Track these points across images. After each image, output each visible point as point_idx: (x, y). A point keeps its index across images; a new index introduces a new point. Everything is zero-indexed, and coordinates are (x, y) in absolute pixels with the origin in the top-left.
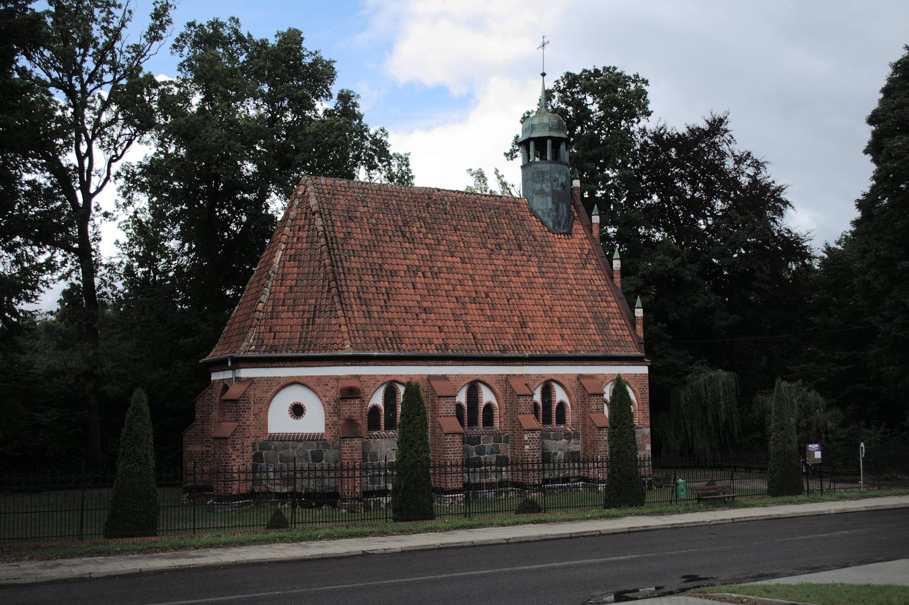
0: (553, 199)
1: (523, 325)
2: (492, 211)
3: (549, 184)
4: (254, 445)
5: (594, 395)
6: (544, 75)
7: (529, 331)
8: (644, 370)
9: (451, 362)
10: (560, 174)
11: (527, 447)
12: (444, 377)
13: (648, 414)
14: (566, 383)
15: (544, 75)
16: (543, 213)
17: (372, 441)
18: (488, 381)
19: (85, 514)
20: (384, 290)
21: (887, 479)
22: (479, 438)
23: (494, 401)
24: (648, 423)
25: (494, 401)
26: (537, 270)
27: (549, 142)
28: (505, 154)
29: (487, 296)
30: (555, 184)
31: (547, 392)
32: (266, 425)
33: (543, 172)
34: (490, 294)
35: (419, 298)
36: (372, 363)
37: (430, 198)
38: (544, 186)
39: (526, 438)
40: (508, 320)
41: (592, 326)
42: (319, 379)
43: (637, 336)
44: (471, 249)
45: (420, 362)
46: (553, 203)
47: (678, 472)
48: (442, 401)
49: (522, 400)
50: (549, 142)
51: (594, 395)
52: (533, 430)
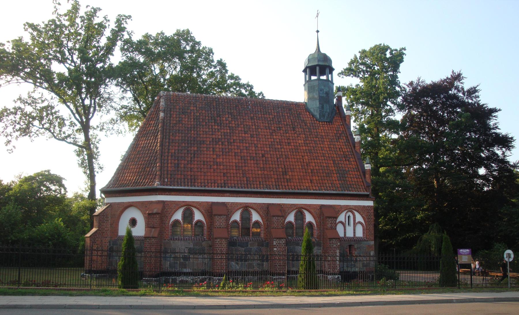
0: (319, 101)
1: (285, 173)
2: (280, 109)
3: (317, 93)
4: (110, 242)
5: (329, 217)
6: (318, 31)
7: (288, 177)
8: (370, 203)
9: (228, 194)
10: (325, 86)
11: (275, 249)
12: (224, 204)
13: (373, 232)
14: (312, 211)
15: (318, 31)
16: (314, 110)
17: (172, 242)
18: (254, 207)
19: (17, 279)
20: (193, 152)
21: (168, 291)
22: (247, 243)
23: (260, 220)
24: (373, 238)
25: (260, 220)
26: (303, 142)
27: (318, 68)
28: (100, 9)
29: (263, 156)
30: (321, 92)
31: (300, 216)
32: (118, 233)
33: (314, 86)
34: (266, 156)
35: (215, 156)
36: (173, 193)
37: (238, 102)
38: (314, 94)
39: (275, 244)
40: (275, 170)
41: (335, 175)
42: (143, 203)
43: (366, 182)
44: (260, 130)
45: (188, 193)
46: (320, 104)
47: (21, 270)
48: (216, 217)
49: (275, 219)
50: (318, 68)
51: (329, 217)
52: (280, 238)
